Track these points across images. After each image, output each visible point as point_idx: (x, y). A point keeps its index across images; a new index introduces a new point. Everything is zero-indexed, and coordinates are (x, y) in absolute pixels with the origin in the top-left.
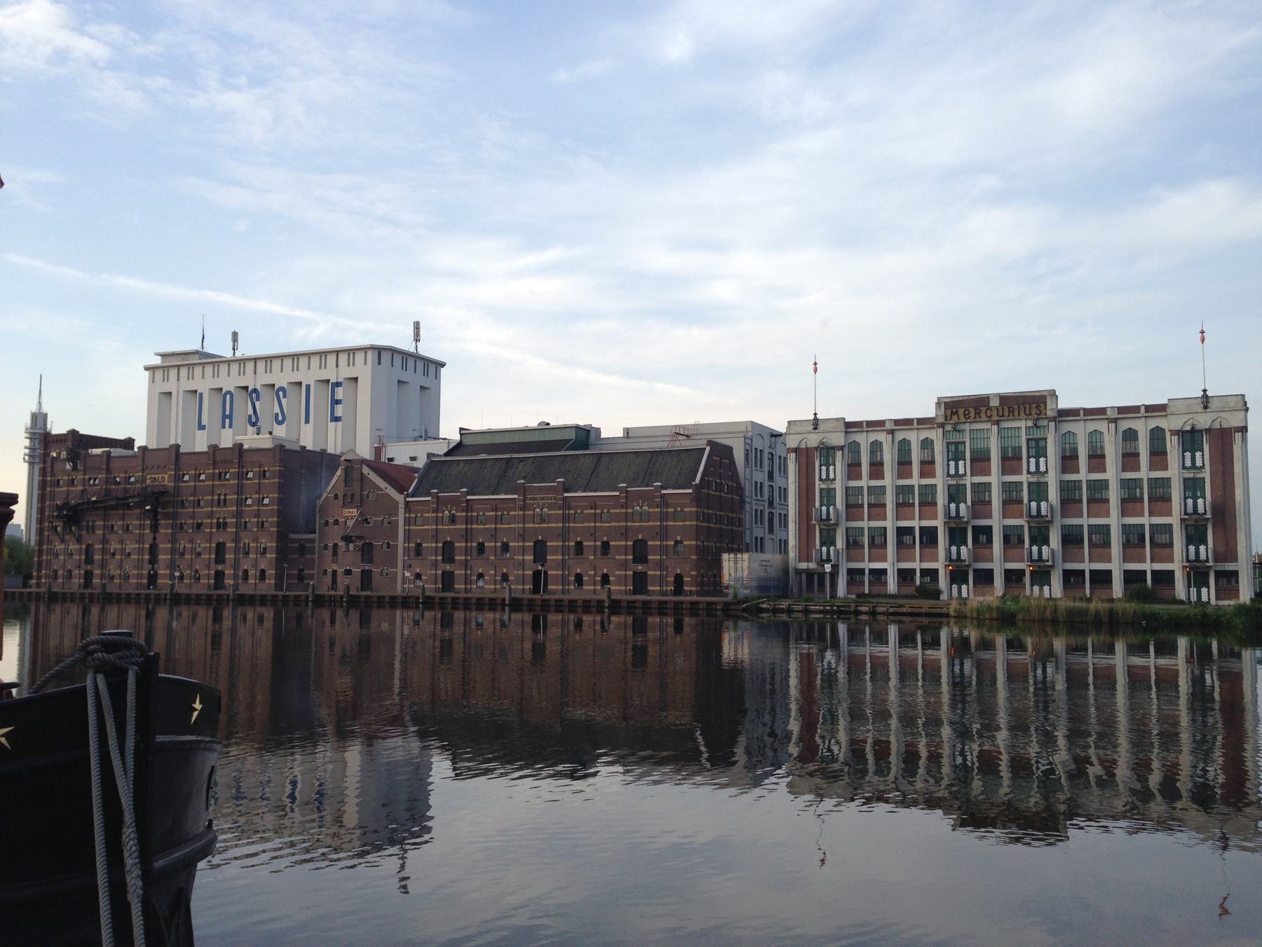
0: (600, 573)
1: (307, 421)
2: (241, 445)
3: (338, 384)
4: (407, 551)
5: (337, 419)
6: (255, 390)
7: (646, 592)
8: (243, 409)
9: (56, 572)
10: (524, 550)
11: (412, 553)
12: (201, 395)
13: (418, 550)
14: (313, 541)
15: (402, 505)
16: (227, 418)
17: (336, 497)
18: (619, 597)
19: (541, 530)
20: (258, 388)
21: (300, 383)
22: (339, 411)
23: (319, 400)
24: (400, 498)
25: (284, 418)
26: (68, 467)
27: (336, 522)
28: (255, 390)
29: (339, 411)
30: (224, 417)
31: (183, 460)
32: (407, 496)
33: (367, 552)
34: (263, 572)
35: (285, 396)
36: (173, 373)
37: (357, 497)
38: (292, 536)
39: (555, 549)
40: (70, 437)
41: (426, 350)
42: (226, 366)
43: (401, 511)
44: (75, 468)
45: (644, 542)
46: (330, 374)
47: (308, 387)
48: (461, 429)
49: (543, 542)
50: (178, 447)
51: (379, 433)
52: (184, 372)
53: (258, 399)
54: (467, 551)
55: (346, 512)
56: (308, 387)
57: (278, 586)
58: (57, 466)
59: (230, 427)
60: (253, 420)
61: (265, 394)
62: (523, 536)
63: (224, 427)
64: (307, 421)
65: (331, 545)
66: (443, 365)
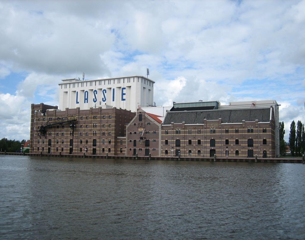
0: (37, 147)
1: (113, 100)
2: (101, 108)
3: (124, 88)
4: (162, 143)
5: (123, 100)
6: (95, 91)
7: (253, 156)
8: (91, 96)
9: (38, 148)
10: (206, 142)
11: (164, 144)
12: (77, 92)
13: (167, 142)
14: (125, 139)
15: (160, 127)
16: (86, 100)
17: (135, 124)
18: (219, 158)
19: (214, 136)
20: (97, 90)
21: (111, 88)
22: (124, 97)
23: (118, 93)
24: (159, 125)
25: (96, 100)
26: (42, 114)
27: (135, 133)
28: (95, 91)
29: (124, 97)
30: (85, 99)
31: (80, 112)
32: (162, 124)
33: (147, 143)
34: (109, 149)
35: (106, 92)
36: (68, 85)
37: (144, 124)
38: (118, 137)
39: (219, 143)
40: (41, 105)
41: (150, 77)
42: (127, 79)
43: (160, 130)
44: (44, 115)
45: (214, 140)
46: (94, 87)
47: (114, 89)
48: (174, 102)
49: (214, 140)
50: (79, 108)
51: (139, 104)
52: (72, 85)
53: (96, 93)
54: (54, 142)
55: (140, 130)
56: (114, 89)
57: (115, 154)
58: (38, 115)
59: (87, 102)
60: (95, 100)
61: (108, 91)
62: (206, 138)
63: (85, 102)
64: (113, 100)
65: (133, 140)
66: (154, 83)
